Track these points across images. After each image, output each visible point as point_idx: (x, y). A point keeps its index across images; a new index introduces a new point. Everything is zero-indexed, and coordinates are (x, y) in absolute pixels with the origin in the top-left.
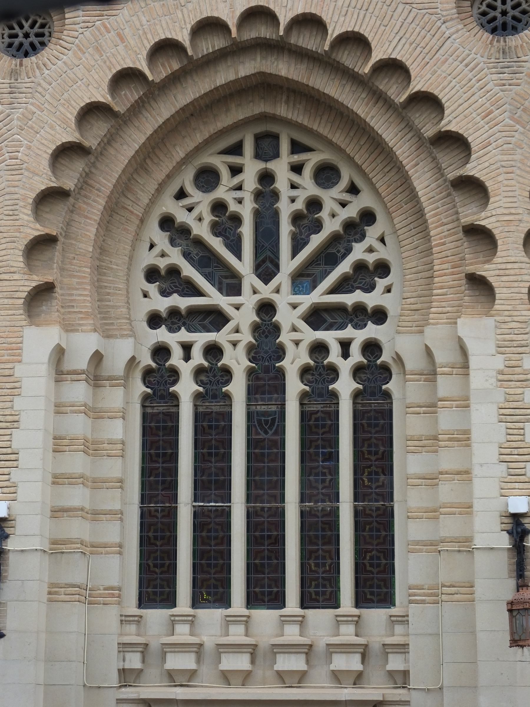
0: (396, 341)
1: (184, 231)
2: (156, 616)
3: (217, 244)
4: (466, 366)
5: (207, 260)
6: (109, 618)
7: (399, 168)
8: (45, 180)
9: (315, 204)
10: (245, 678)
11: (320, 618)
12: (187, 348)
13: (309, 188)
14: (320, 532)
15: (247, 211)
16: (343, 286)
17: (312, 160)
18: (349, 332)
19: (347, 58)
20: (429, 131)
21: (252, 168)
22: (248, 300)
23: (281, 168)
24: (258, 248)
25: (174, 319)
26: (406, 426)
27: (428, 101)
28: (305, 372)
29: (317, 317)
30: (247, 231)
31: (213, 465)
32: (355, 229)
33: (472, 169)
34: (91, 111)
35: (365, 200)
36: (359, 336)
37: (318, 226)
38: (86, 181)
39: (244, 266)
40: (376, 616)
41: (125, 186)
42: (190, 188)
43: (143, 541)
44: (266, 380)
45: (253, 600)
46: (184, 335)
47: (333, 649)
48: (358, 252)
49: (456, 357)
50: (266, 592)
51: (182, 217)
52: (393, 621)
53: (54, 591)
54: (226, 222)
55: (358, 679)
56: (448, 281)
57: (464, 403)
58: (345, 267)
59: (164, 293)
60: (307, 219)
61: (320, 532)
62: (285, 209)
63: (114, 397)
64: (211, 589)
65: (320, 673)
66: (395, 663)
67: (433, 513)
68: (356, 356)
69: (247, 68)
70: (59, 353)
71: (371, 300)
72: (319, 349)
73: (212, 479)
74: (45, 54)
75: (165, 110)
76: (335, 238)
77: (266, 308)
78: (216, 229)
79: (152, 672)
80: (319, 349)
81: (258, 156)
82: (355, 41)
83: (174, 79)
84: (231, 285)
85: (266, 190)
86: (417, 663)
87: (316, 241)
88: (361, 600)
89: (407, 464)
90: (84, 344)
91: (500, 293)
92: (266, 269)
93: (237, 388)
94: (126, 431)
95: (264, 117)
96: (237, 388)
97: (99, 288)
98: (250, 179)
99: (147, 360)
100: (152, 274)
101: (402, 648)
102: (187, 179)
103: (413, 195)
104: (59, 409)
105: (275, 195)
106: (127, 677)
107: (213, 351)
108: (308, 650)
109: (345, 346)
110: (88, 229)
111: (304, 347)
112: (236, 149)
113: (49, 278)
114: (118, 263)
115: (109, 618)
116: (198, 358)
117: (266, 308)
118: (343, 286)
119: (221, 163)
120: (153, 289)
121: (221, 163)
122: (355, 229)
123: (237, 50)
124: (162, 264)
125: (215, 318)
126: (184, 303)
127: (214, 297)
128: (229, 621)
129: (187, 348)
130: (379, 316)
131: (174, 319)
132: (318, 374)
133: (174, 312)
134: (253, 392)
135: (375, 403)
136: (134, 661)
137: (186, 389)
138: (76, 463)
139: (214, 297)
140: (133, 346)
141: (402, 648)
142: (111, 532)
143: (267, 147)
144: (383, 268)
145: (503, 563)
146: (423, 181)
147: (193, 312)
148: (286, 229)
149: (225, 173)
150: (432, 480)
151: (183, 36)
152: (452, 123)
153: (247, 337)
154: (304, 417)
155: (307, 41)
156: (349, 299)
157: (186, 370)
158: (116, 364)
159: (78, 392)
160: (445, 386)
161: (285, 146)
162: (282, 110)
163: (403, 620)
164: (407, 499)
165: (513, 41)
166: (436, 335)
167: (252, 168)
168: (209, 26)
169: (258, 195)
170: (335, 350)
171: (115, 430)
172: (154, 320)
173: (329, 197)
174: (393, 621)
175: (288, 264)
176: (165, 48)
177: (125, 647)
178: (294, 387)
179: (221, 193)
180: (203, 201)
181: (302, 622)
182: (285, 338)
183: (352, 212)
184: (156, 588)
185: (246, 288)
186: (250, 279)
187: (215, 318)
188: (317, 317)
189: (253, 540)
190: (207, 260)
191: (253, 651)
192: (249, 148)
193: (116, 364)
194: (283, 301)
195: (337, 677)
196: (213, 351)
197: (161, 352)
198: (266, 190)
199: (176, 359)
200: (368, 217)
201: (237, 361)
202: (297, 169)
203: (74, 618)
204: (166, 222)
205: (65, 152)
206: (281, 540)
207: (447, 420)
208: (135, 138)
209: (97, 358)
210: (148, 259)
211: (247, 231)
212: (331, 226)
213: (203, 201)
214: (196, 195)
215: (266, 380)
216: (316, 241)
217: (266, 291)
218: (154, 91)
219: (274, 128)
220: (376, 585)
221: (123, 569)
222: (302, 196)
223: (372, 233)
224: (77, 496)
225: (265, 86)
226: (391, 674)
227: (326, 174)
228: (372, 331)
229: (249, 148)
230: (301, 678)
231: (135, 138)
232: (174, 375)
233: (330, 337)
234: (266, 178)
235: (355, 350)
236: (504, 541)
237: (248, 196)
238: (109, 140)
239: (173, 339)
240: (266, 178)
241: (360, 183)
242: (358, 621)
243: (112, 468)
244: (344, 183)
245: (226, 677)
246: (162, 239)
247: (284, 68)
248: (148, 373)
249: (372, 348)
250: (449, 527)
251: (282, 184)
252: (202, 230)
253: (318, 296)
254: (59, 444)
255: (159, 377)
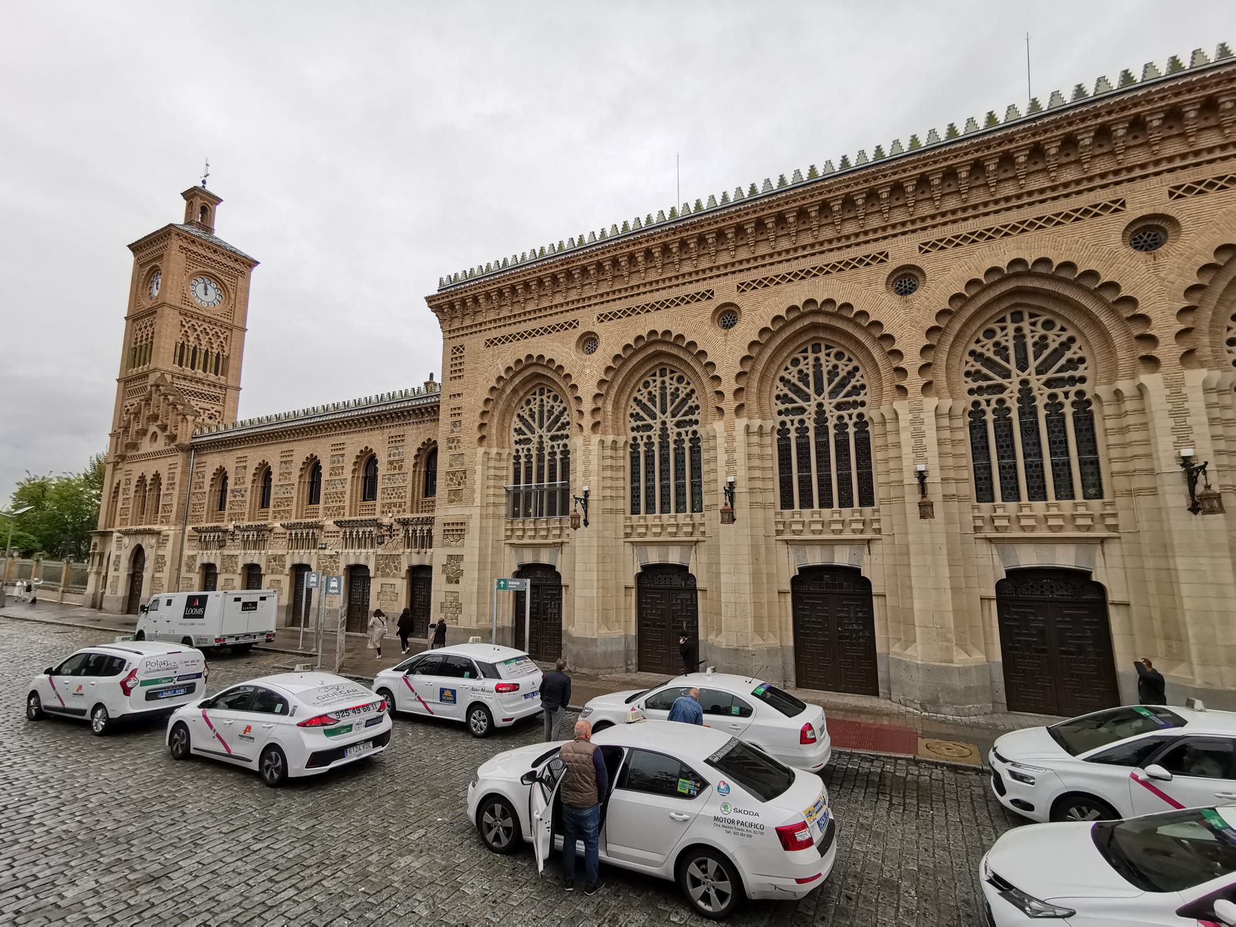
0: (870, 412)
1: (789, 381)
2: (787, 512)
3: (800, 385)
4: (897, 418)
5: (797, 391)
6: (771, 513)
7: (867, 350)
8: (738, 369)
9: (836, 367)
10: (820, 532)
11: (846, 511)
12: (792, 421)
13: (833, 361)
14: (845, 481)
15: (811, 372)
16: (848, 395)
17: (676, 375)
18: (1067, 388)
19: (844, 313)
20: (878, 335)
21: (811, 356)
22: (813, 403)
23: (822, 355)
24: (815, 385)
25: (980, 390)
26: (875, 442)
27: (877, 324)
28: (675, 442)
29: (678, 425)
30: (811, 379)
31: (804, 460)
32: (851, 374)
33: (896, 347)
34: (753, 344)
35: (855, 363)
36: (855, 412)
37: (837, 374)
38: (753, 368)
39: (811, 391)
40: (868, 510)
41: (767, 368)
42: (982, 338)
43: (781, 487)
44: (821, 430)
45: (1031, 498)
46: (791, 417)
47: (851, 522)
48: (853, 382)
49: (893, 416)
50: (826, 503)
51: (787, 377)
52: (874, 511)
53: (751, 504)
54: (803, 377)
55: (862, 532)
56: (887, 387)
57: (898, 432)
58: (849, 388)
59: (974, 381)
60: (675, 395)
61: (845, 481)
62: (825, 370)
63: (768, 440)
64: (806, 502)
65: (848, 529)
66: (875, 526)
67: (888, 472)
68: (855, 419)
69: (807, 322)
70: (748, 427)
71: (693, 417)
72: (840, 418)
73: (804, 465)
74: (738, 325)
75: (779, 340)
76: (844, 378)
77: (820, 405)
78: (649, 400)
79: (787, 530)
80: (840, 418)
81: (813, 352)
82: (848, 306)
83: (781, 329)
84: (807, 398)
85: (1019, 335)
86: (884, 525)
87: (837, 380)
88: (821, 506)
89: (876, 456)
90: (757, 422)
91: (910, 391)
92: (819, 391)
93: (811, 434)
94: (772, 451)
95: (814, 338)
96: (811, 434)
97: (760, 404)
98: (811, 361)
99: (778, 427)
100: (778, 397)
101: (878, 520)
102: (641, 386)
103: (873, 359)
104: (749, 445)
105: (1024, 336)
106: (778, 532)
107: (802, 422)
108: (843, 522)
109: (850, 416)
110: (755, 384)
111: (1045, 396)
112: (806, 351)
113: (1191, 346)
114: (766, 395)
115: (771, 513)
116: (796, 425)
117: (820, 405)
118: (848, 395)
119: (800, 356)
120: (779, 402)
121: (800, 356)
122: (851, 374)
123: (803, 316)
124: (781, 394)
125: (802, 410)
126: (790, 406)
127: (800, 403)
128: (813, 513)
129: (792, 421)
130: (863, 404)
131: (787, 412)
132: (679, 441)
133: (787, 409)
134: (816, 435)
135: (863, 435)
136: (781, 527)
137: (793, 435)
138: (756, 463)
139: (800, 403)
140: (772, 423)
141: (703, 524)
142: (769, 485)
143: (817, 348)
144: (863, 387)
145: (916, 489)
146: (877, 354)
147: (793, 409)
148: (825, 377)
149: (998, 331)
150: (886, 461)
151: (783, 314)
152: (886, 331)
153: (813, 416)
154: (836, 442)
155: (829, 309)
156: (850, 399)
157: (792, 429)
158: (768, 428)
159: (945, 422)
160: (889, 427)
161: (823, 347)
162: (821, 335)
163: (878, 511)
164: (877, 469)
165: (910, 297)
166: (885, 409)
167: (811, 356)
168: (793, 308)
169: (814, 366)
170: (847, 417)
171: (769, 451)
172: (971, 392)
173: (841, 364)
174: (874, 511)
175: (827, 389)
176: (777, 319)
177: (625, 526)
178: (832, 432)
179: (800, 367)
180: (794, 370)
181: (840, 513)
182: (669, 432)
183: (850, 368)
184: (787, 503)
185: (1027, 372)
186: (813, 395)
187: (802, 410)
188: (839, 407)
189: (820, 485)
190: (797, 391)
191: (843, 522)
192: (810, 350)
193: (768, 428)
194: (826, 402)
195: (854, 531)
196: (802, 422)
197: (783, 423)
198: (1019, 335)
199: (789, 425)
200: (856, 369)
201: (811, 424)
202: (828, 355)
203: (759, 513)
204: (782, 379)
205: (745, 359)
206: (830, 485)
207: (891, 439)
208: (769, 352)
209: (761, 427)
210: (776, 392)
211: (811, 379)
212: (842, 374)
213: (794, 370)
214: (792, 368)
215: (821, 430)
216: (837, 380)
217: (819, 399)
218: (774, 334)
219: (1019, 309)
220: (867, 498)
221: (775, 497)
222: (831, 364)
223: (858, 375)
224: (757, 474)
225: (815, 327)
226: (874, 530)
227: (839, 356)
228: (860, 409)
229: (810, 350)
230: (841, 532)
231: (769, 352)
232: (846, 425)
233: (682, 430)
234: (817, 359)
235: (854, 417)
236: (916, 481)
237: (810, 366)
238: (760, 353)
239: (982, 399)
240: (817, 359)
241: (1065, 326)
242: (840, 513)
243: (769, 464)
244: (1058, 327)
245: (813, 532)
246: (780, 385)
247: (820, 320)
248: (779, 431)
249: (860, 416)
250: (894, 477)
251: (823, 361)
252: (795, 380)
253: (839, 399)
254: (750, 456)
255: (783, 432)
